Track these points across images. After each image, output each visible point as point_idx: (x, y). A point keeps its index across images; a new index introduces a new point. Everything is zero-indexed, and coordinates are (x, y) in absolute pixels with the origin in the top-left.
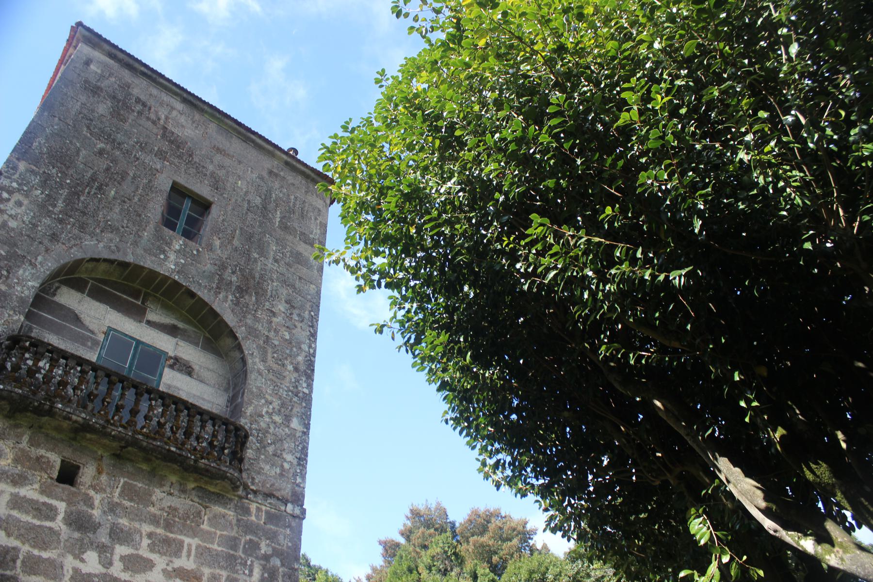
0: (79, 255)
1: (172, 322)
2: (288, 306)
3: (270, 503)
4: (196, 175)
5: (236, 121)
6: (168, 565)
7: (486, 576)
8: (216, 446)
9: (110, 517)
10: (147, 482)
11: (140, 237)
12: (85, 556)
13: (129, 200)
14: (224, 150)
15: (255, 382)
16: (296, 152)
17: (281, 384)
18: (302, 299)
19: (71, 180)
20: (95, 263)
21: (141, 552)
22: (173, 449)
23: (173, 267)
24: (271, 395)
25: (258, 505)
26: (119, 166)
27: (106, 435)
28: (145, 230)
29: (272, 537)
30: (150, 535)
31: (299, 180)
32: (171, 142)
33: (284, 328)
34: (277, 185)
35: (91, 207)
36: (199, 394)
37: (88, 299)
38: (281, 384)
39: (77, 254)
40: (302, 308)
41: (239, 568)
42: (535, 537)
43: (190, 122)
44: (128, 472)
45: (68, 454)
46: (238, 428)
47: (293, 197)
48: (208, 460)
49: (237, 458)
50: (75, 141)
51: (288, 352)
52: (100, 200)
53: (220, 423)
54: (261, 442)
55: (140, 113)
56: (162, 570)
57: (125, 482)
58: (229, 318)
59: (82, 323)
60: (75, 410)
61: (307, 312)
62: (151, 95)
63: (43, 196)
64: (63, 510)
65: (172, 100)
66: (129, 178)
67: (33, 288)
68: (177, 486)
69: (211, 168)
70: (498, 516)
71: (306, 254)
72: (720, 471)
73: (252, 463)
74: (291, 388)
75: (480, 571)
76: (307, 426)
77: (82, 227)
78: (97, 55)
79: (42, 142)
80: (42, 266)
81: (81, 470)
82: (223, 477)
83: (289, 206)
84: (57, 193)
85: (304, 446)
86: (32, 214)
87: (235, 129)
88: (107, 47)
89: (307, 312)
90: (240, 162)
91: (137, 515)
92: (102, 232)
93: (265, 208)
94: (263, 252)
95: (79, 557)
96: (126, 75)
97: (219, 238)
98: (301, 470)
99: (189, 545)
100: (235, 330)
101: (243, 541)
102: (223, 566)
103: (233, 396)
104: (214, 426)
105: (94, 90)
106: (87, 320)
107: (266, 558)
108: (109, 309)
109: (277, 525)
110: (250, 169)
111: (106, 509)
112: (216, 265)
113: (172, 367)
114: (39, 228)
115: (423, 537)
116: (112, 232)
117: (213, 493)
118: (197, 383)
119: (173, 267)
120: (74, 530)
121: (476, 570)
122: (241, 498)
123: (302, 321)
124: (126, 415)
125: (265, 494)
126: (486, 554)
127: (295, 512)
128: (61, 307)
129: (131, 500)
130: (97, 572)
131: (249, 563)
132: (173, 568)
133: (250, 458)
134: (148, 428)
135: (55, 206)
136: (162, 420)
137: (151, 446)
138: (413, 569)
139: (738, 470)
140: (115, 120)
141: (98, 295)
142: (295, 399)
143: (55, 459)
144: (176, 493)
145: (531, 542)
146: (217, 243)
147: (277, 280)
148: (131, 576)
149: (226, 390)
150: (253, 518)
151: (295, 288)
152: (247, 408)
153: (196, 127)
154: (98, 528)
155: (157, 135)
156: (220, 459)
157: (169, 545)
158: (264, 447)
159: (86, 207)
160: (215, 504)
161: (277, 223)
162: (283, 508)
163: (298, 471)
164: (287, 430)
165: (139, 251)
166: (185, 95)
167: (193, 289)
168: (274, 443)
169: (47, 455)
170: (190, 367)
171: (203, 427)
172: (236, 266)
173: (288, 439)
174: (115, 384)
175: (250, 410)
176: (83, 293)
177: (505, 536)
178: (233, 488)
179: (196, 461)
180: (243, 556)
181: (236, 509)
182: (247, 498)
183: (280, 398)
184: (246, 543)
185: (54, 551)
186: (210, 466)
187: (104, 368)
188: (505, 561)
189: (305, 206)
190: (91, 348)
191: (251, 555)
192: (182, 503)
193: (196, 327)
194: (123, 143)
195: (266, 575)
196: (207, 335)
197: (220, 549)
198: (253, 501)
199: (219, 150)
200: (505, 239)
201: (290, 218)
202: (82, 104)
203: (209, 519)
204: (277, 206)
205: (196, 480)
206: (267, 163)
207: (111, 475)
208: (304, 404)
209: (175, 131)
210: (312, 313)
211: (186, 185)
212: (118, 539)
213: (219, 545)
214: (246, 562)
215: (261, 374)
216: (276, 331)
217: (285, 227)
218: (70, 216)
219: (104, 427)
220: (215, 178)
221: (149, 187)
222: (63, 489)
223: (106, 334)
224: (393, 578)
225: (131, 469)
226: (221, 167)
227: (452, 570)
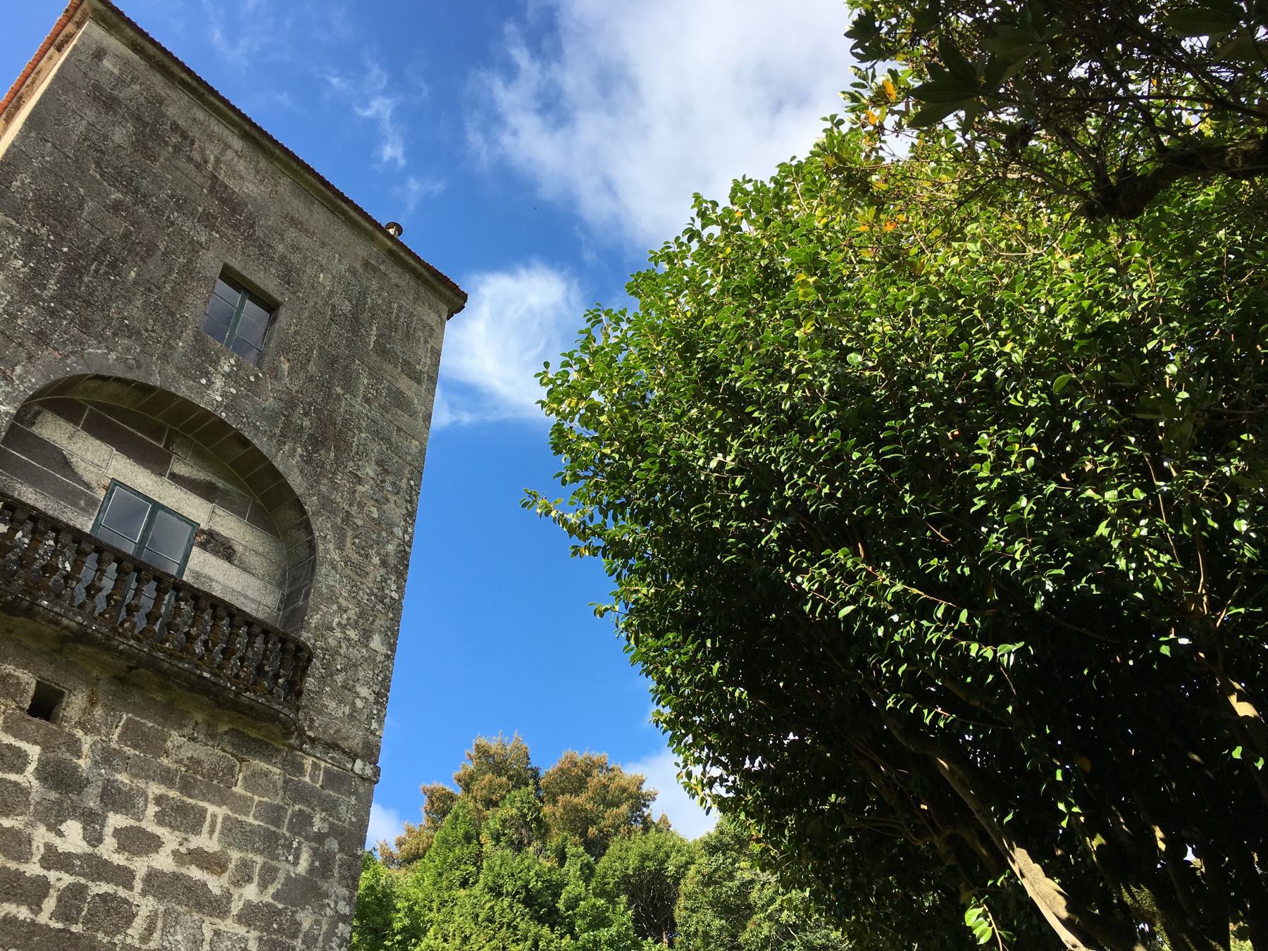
0: (79, 369)
1: (208, 479)
2: (379, 469)
3: (332, 758)
4: (258, 259)
5: (321, 179)
6: (181, 844)
7: (579, 857)
8: (267, 673)
9: (103, 771)
10: (161, 720)
11: (171, 348)
12: (63, 828)
13: (158, 288)
14: (301, 223)
15: (327, 578)
16: (399, 229)
17: (362, 583)
18: (400, 461)
19: (69, 247)
20: (100, 382)
21: (144, 825)
22: (206, 674)
23: (219, 399)
24: (346, 599)
25: (315, 760)
26: (143, 231)
27: (108, 648)
28: (179, 337)
29: (330, 807)
30: (159, 800)
31: (404, 280)
32: (224, 201)
33: (372, 502)
34: (374, 285)
35: (100, 295)
36: (239, 589)
37: (84, 434)
38: (362, 583)
39: (75, 366)
40: (398, 473)
41: (281, 852)
42: (653, 805)
43: (253, 171)
44: (134, 704)
45: (48, 673)
46: (301, 647)
47: (396, 305)
48: (255, 692)
49: (294, 689)
50: (76, 184)
51: (374, 536)
52: (114, 284)
53: (276, 639)
54: (326, 667)
55: (177, 149)
56: (173, 851)
57: (129, 719)
58: (296, 481)
59: (73, 470)
60: (67, 610)
61: (404, 480)
62: (194, 120)
63: (26, 269)
64: (36, 757)
65: (226, 132)
66: (159, 253)
67: (6, 416)
68: (203, 728)
69: (281, 248)
70: (602, 768)
71: (409, 394)
72: (1013, 861)
73: (312, 698)
74: (375, 591)
75: (570, 850)
76: (392, 647)
77: (85, 326)
78: (113, 43)
79: (26, 181)
80: (22, 382)
81: (65, 699)
82: (274, 718)
83: (390, 319)
84: (48, 267)
85: (386, 676)
86: (8, 298)
87: (318, 191)
88: (130, 33)
89: (404, 480)
90: (323, 245)
91: (142, 769)
92: (115, 335)
93: (356, 319)
94: (349, 386)
95: (54, 828)
96: (158, 82)
97: (288, 360)
98: (379, 710)
99: (214, 816)
100: (303, 500)
101: (290, 812)
102: (258, 848)
103: (289, 595)
104: (266, 642)
105: (107, 102)
106: (81, 468)
107: (320, 838)
108: (115, 452)
109: (339, 791)
110: (337, 256)
111: (98, 758)
112: (281, 400)
113: (203, 546)
114: (19, 322)
115: (490, 788)
116: (129, 337)
117: (254, 740)
118: (239, 571)
119: (219, 399)
120: (50, 788)
121: (564, 847)
122: (292, 748)
123: (397, 493)
124: (140, 621)
125: (326, 743)
126: (579, 822)
127: (366, 772)
128: (43, 443)
129: (135, 747)
130: (79, 851)
131: (295, 845)
132: (188, 849)
133: (310, 691)
134: (172, 643)
135: (44, 287)
136: (194, 631)
137: (176, 669)
138: (472, 837)
139: (1037, 866)
140: (138, 157)
141: (102, 429)
142: (379, 607)
143: (28, 680)
144: (201, 737)
145: (646, 811)
146: (286, 366)
147: (367, 430)
148: (127, 859)
149: (279, 585)
150: (307, 779)
151: (391, 444)
152: (312, 617)
153: (261, 181)
154: (86, 786)
155: (202, 187)
156: (271, 692)
157: (186, 816)
158: (332, 675)
159: (91, 294)
160: (255, 757)
161: (372, 344)
162: (349, 766)
163: (375, 712)
164: (364, 650)
165: (171, 370)
166: (247, 127)
167: (246, 434)
168: (344, 669)
169: (16, 674)
170: (230, 547)
171: (250, 644)
172: (310, 404)
173: (365, 666)
174: (128, 573)
175: (315, 620)
176: (77, 424)
177: (609, 797)
178: (284, 734)
179: (237, 694)
180: (288, 834)
181: (284, 765)
182: (301, 750)
183: (359, 604)
184: (292, 817)
185: (19, 818)
186: (257, 702)
187: (113, 548)
188: (607, 836)
189: (411, 322)
190: (84, 510)
191: (299, 834)
192: (207, 753)
193: (241, 487)
194: (151, 196)
195: (317, 864)
196: (259, 501)
197: (256, 823)
198: (309, 754)
199: (294, 222)
200: (792, 551)
201: (390, 337)
202: (89, 123)
203: (245, 778)
204: (372, 318)
205: (231, 722)
206: (362, 250)
207: (109, 708)
208: (391, 615)
209: (230, 183)
210: (412, 483)
211: (244, 273)
212: (113, 804)
213: (255, 818)
214: (291, 844)
215: (335, 568)
216: (361, 506)
217: (382, 351)
218: (68, 307)
219: (108, 638)
220: (286, 265)
221: (188, 270)
222: (38, 727)
223: (109, 490)
224: (441, 848)
225: (138, 700)
226: (296, 248)
227: (529, 844)
